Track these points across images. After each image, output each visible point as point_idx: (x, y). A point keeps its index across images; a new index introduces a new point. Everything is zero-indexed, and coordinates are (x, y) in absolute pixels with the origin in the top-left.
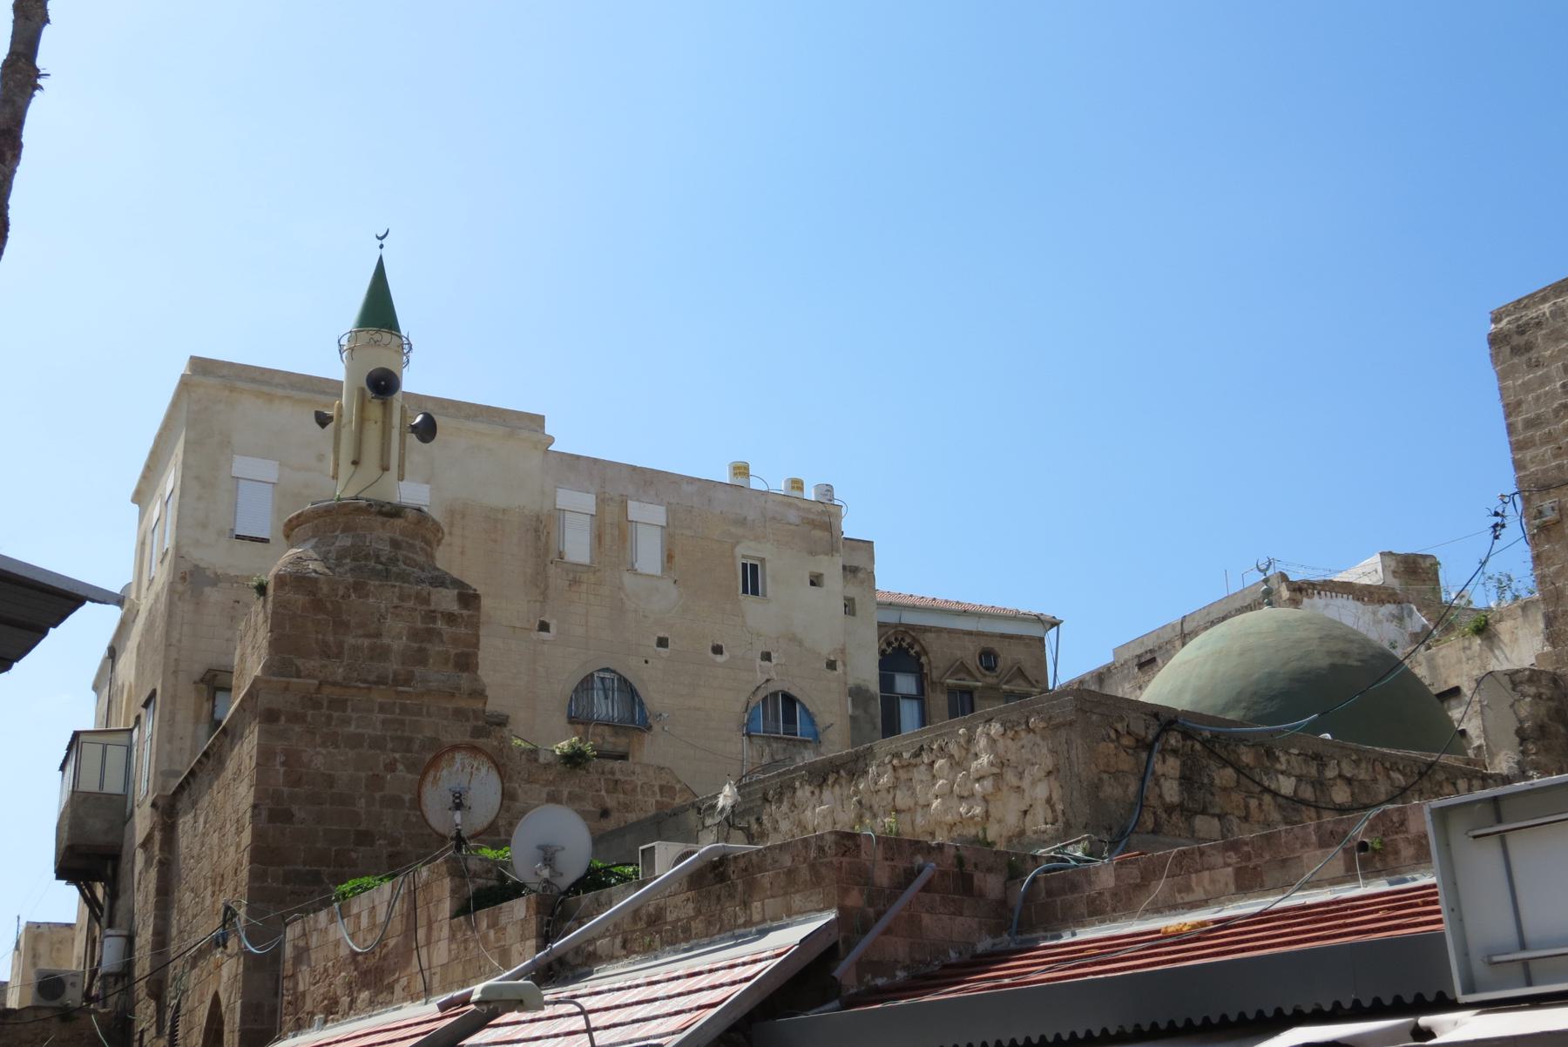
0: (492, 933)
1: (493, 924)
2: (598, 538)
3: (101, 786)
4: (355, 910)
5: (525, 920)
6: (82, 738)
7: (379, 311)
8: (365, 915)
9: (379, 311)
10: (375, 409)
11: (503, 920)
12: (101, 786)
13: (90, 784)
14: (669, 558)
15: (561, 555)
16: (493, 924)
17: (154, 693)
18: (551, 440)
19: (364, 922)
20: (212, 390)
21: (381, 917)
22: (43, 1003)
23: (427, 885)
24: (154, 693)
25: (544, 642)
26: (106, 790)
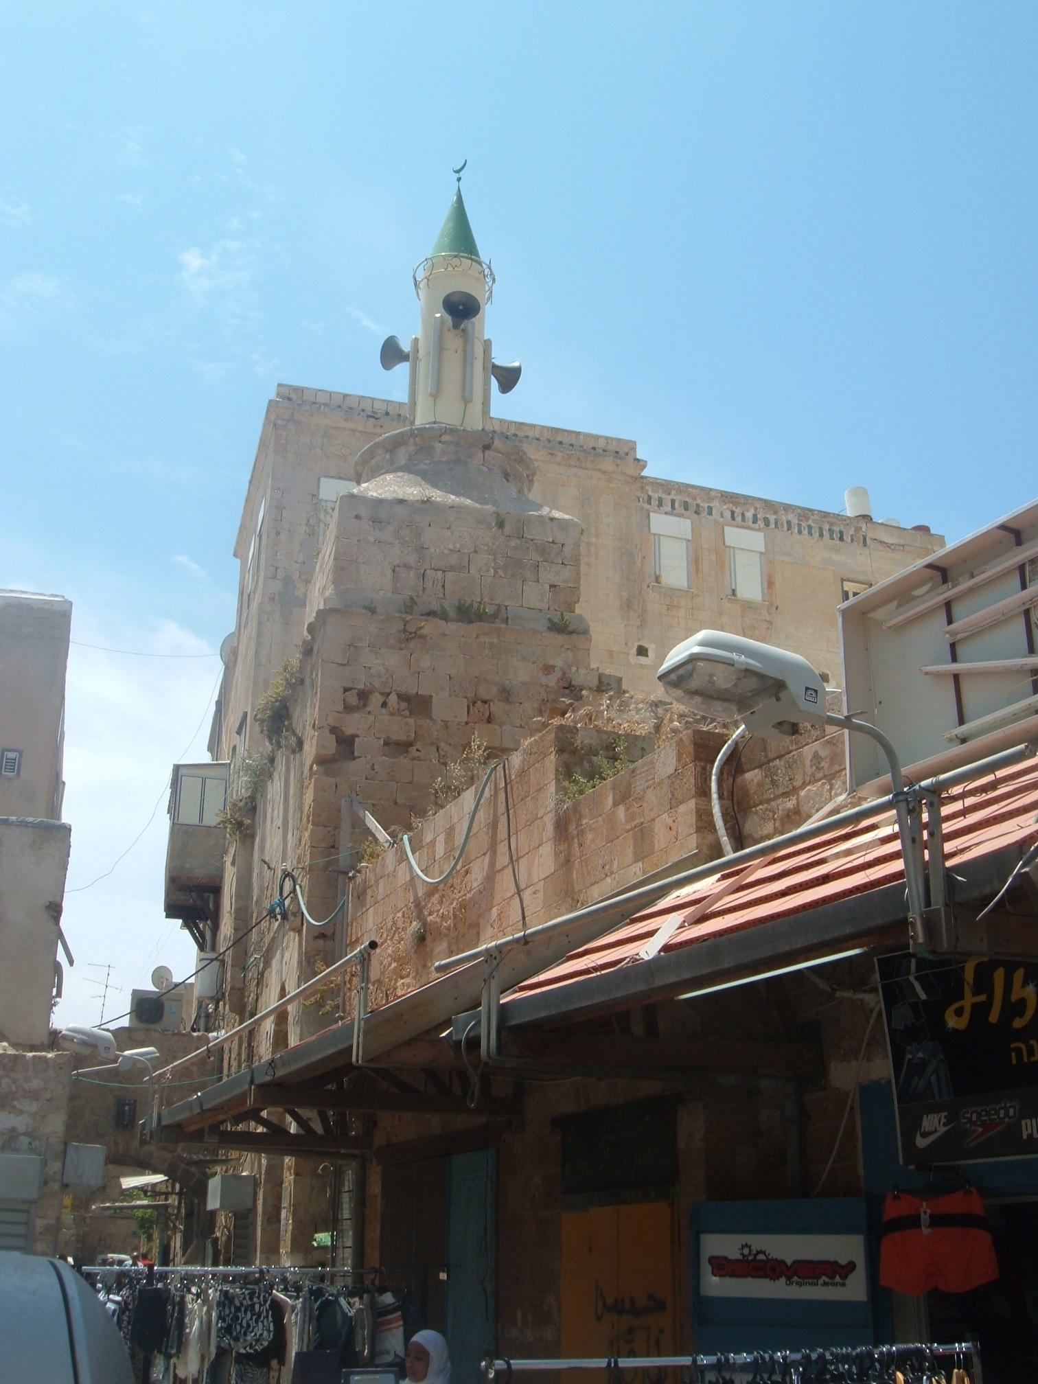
0: (621, 812)
1: (623, 797)
2: (695, 562)
3: (201, 819)
4: (428, 838)
5: (676, 775)
6: (182, 771)
7: (462, 239)
8: (441, 840)
9: (462, 239)
10: (453, 342)
11: (639, 785)
12: (201, 819)
13: (189, 816)
14: (769, 583)
15: (657, 579)
16: (623, 797)
17: (245, 714)
18: (641, 464)
19: (440, 849)
20: (298, 422)
21: (459, 839)
22: (141, 1025)
23: (523, 773)
24: (245, 714)
25: (642, 666)
26: (205, 822)
